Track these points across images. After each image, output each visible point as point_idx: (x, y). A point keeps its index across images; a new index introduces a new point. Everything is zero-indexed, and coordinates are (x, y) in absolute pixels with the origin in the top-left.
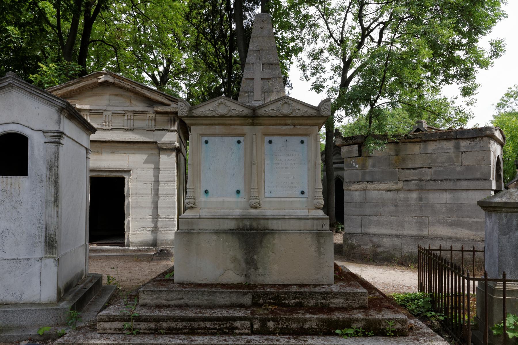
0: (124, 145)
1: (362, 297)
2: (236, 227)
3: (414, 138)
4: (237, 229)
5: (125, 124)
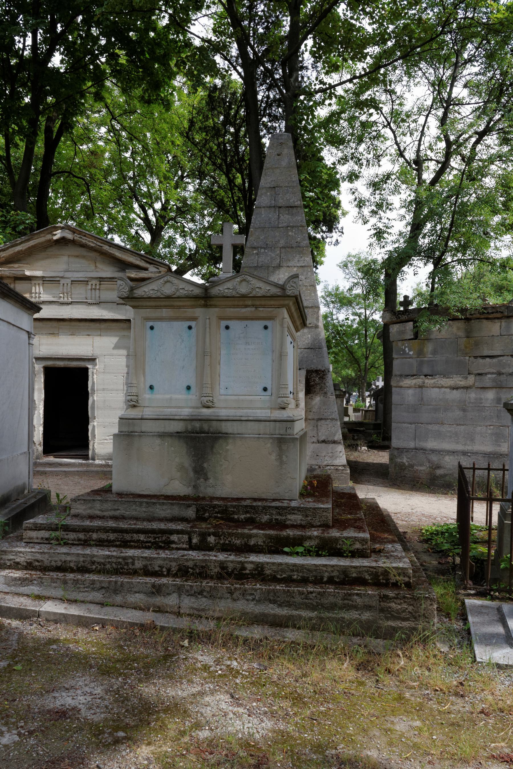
0: (87, 324)
1: (324, 514)
2: (183, 430)
3: (492, 313)
4: (185, 432)
5: (89, 296)
